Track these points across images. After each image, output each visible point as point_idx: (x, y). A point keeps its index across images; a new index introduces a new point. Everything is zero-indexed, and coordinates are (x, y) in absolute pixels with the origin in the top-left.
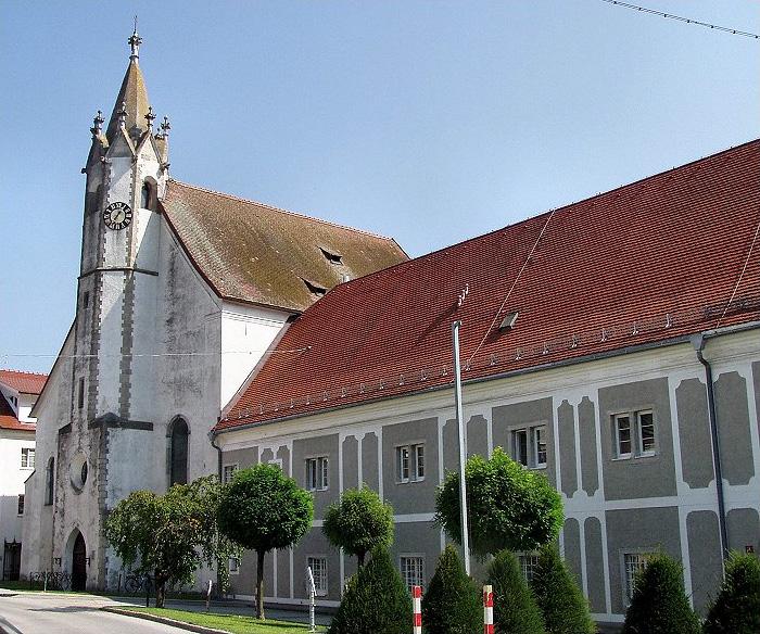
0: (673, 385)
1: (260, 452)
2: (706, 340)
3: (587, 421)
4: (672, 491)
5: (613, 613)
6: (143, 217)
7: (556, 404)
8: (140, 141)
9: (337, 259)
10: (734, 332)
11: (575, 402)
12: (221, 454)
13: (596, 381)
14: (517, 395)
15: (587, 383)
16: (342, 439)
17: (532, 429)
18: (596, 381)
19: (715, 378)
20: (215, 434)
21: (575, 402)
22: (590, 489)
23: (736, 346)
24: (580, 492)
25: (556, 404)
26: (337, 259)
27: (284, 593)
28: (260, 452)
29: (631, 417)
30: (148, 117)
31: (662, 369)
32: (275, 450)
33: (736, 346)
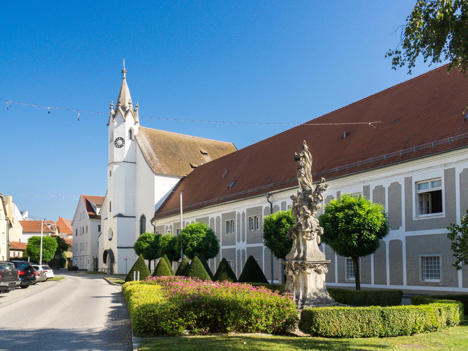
0: (263, 209)
1: (165, 227)
2: (270, 195)
3: (243, 219)
4: (235, 244)
5: (390, 284)
6: (128, 143)
7: (237, 214)
8: (127, 113)
9: (206, 154)
10: (283, 191)
11: (241, 213)
12: (155, 227)
13: (247, 206)
14: (226, 210)
15: (244, 207)
16: (210, 219)
17: (231, 221)
18: (247, 206)
19: (273, 207)
20: (152, 221)
21: (241, 213)
22: (243, 240)
23: (278, 197)
24: (241, 241)
25: (237, 214)
26: (206, 154)
27: (381, 279)
28: (165, 227)
29: (253, 218)
30: (129, 103)
31: (261, 203)
32: (169, 226)
33: (278, 197)
